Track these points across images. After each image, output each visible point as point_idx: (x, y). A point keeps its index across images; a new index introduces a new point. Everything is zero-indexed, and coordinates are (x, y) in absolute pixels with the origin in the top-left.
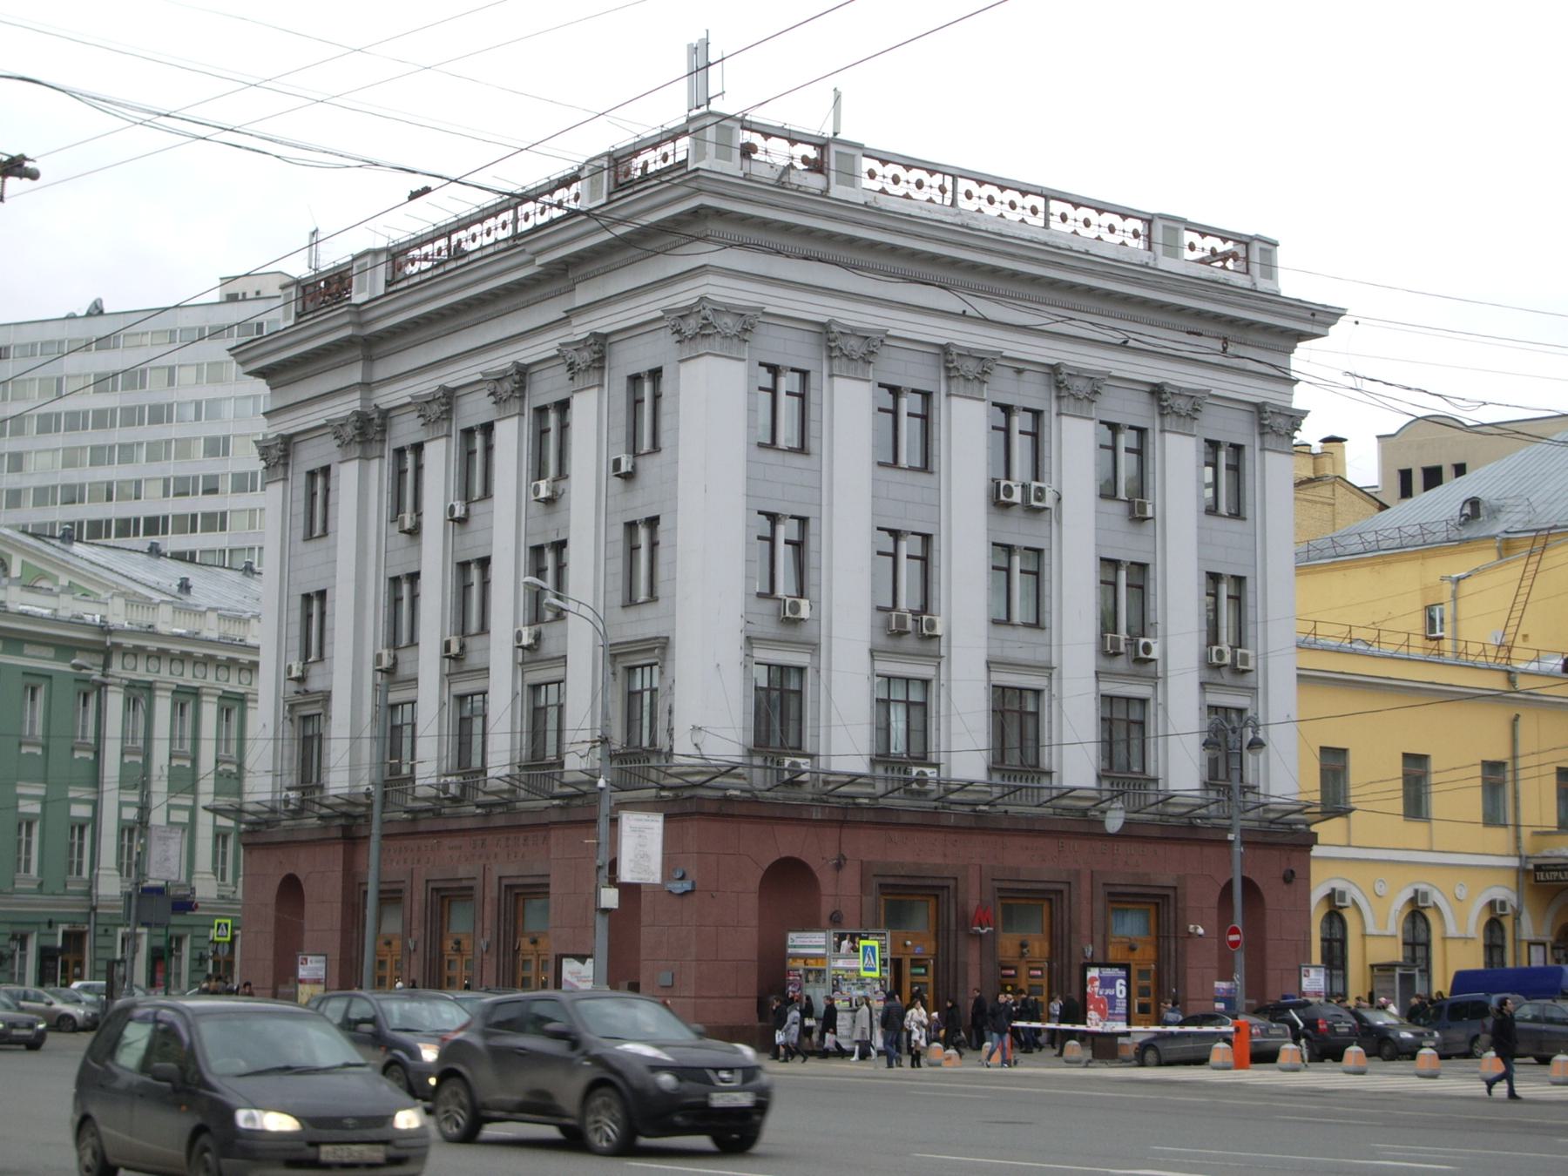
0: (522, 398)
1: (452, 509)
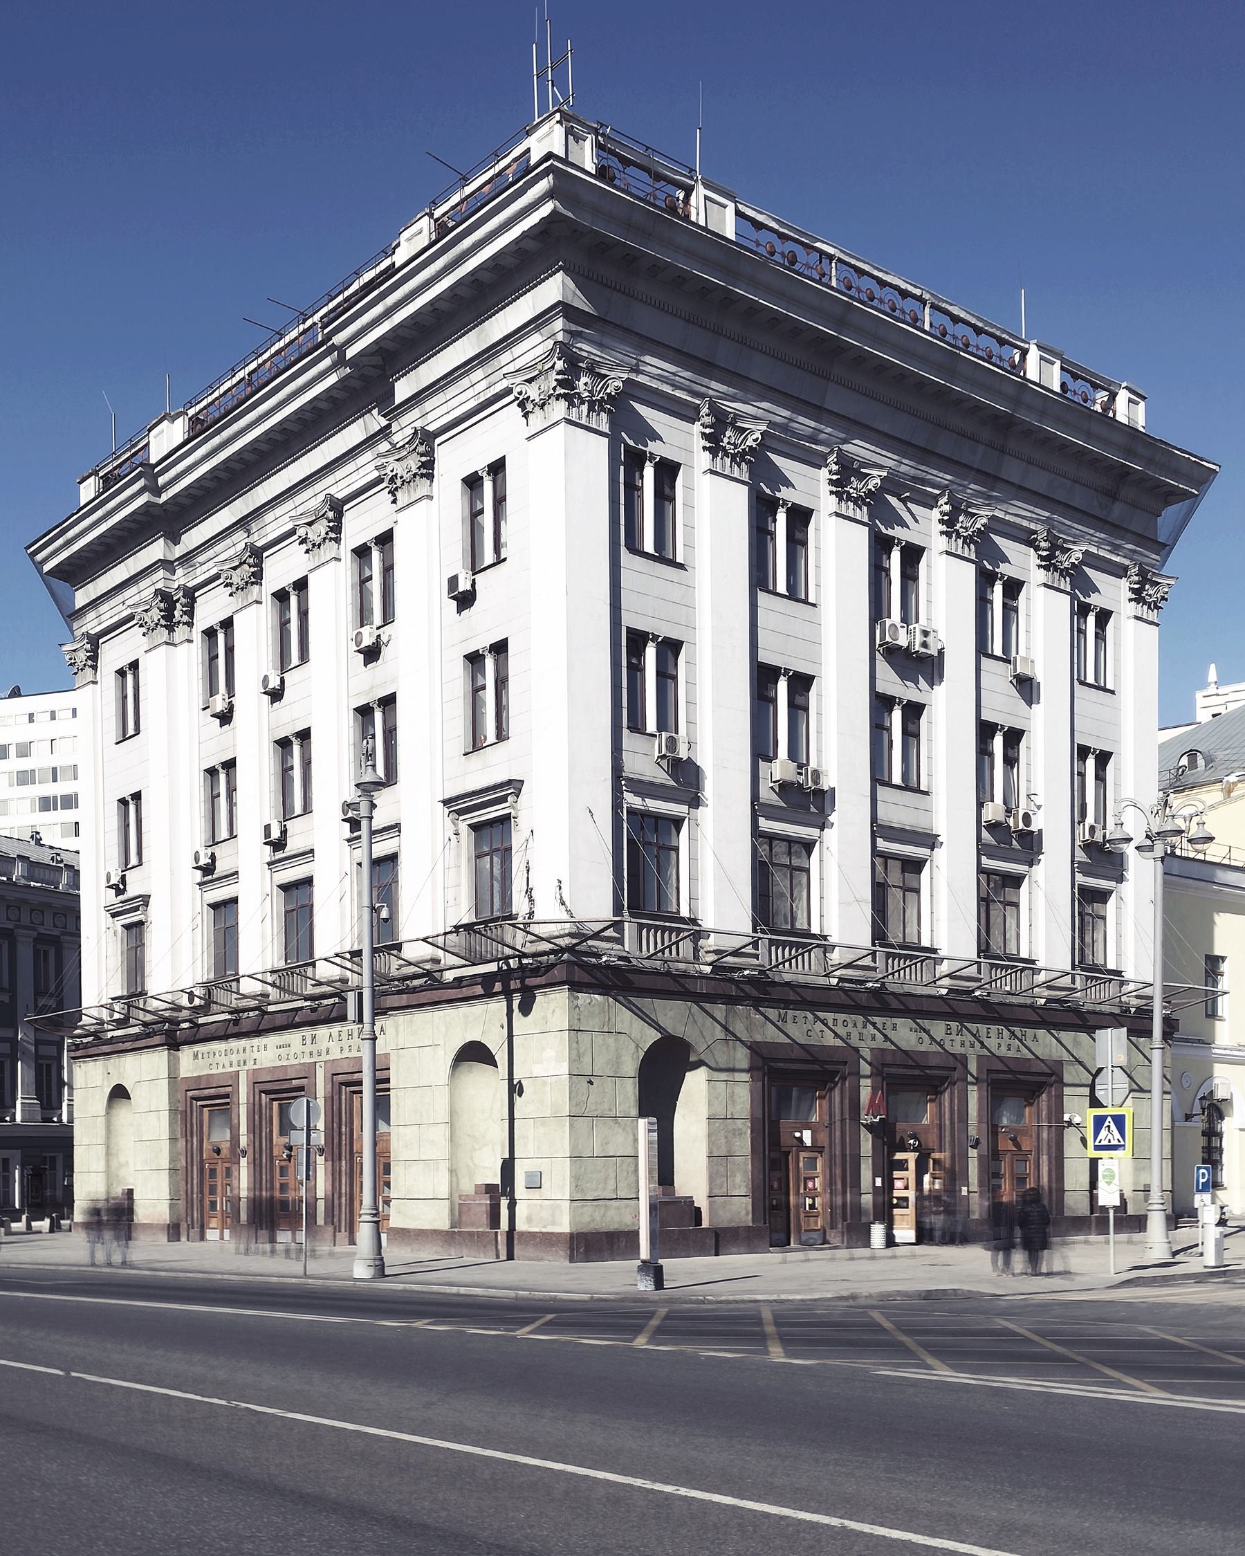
0: (337, 540)
1: (266, 679)
